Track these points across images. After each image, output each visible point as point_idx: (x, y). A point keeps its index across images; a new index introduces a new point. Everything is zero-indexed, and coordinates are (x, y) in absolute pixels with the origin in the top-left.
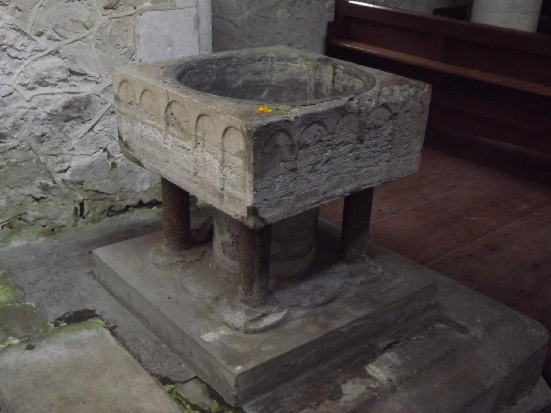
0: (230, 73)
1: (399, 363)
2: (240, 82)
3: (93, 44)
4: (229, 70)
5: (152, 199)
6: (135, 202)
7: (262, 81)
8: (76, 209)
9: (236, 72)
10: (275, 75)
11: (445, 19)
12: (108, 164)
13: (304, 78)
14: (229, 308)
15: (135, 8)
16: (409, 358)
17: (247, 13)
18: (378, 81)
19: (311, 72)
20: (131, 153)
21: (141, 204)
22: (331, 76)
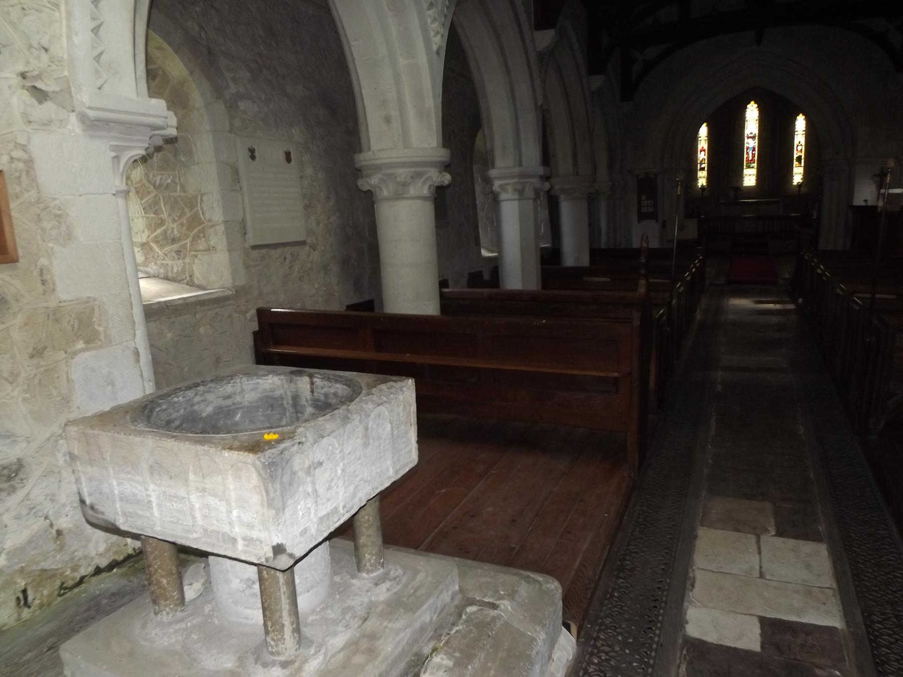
0: (198, 403)
1: (450, 663)
2: (210, 409)
3: (20, 400)
4: (197, 399)
5: (111, 560)
6: (91, 569)
7: (234, 404)
8: (18, 599)
9: (205, 401)
10: (247, 396)
11: (355, 313)
12: (51, 533)
13: (278, 393)
14: (260, 667)
15: (66, 352)
16: (457, 655)
17: (169, 335)
18: (363, 385)
19: (286, 386)
20: (100, 516)
21: (98, 571)
22: (309, 386)
